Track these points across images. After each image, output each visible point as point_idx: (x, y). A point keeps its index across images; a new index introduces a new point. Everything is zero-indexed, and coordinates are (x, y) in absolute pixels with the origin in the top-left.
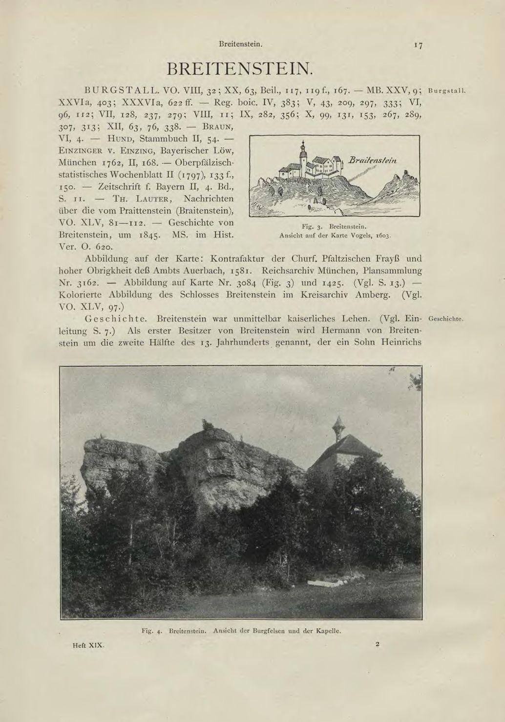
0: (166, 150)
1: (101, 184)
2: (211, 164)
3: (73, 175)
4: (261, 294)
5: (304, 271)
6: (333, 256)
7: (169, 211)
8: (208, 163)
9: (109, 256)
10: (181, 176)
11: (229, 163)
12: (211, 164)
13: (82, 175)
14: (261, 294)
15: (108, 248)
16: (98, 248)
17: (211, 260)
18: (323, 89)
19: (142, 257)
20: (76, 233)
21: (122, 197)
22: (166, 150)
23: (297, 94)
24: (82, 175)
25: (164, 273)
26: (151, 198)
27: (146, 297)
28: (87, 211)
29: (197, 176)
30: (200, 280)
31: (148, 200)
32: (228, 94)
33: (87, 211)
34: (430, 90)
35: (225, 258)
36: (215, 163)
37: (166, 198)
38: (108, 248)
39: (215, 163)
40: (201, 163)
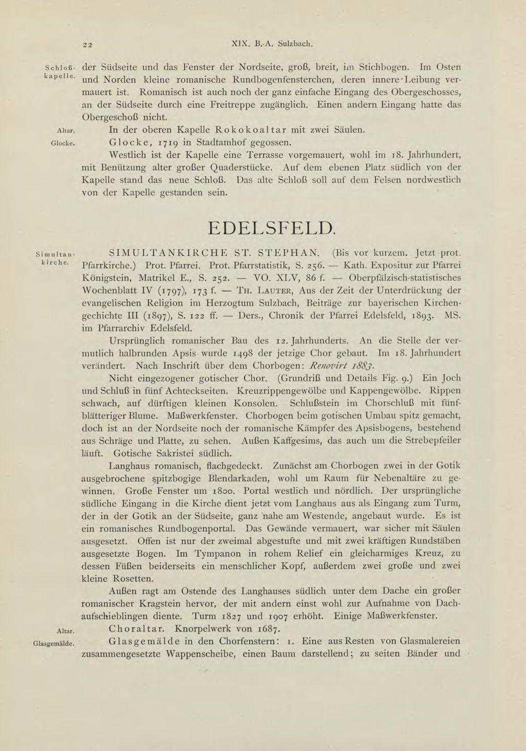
0: (277, 653)
1: (339, 288)
2: (386, 279)
3: (425, 278)
4: (425, 614)
5: (180, 391)
6: (340, 313)
7: (95, 193)
8: (384, 279)
9: (120, 613)
10: (161, 291)
11: (405, 278)
12: (387, 279)
13: (435, 278)
14: (425, 614)
15: (230, 492)
16: (127, 630)
17: (410, 542)
18: (321, 277)
19: (275, 590)
20: (273, 65)
21: (247, 288)
22: (277, 653)
23: (199, 295)
24: (435, 278)
25: (211, 556)
26: (273, 290)
27: (409, 107)
28: (384, 341)
29: (178, 292)
30: (197, 77)
31: (270, 291)
32: (280, 282)
33: (384, 341)
34: (257, 43)
35: (94, 192)
36: (391, 278)
37: (288, 290)
38: (230, 492)
39: (391, 278)
40: (376, 278)
